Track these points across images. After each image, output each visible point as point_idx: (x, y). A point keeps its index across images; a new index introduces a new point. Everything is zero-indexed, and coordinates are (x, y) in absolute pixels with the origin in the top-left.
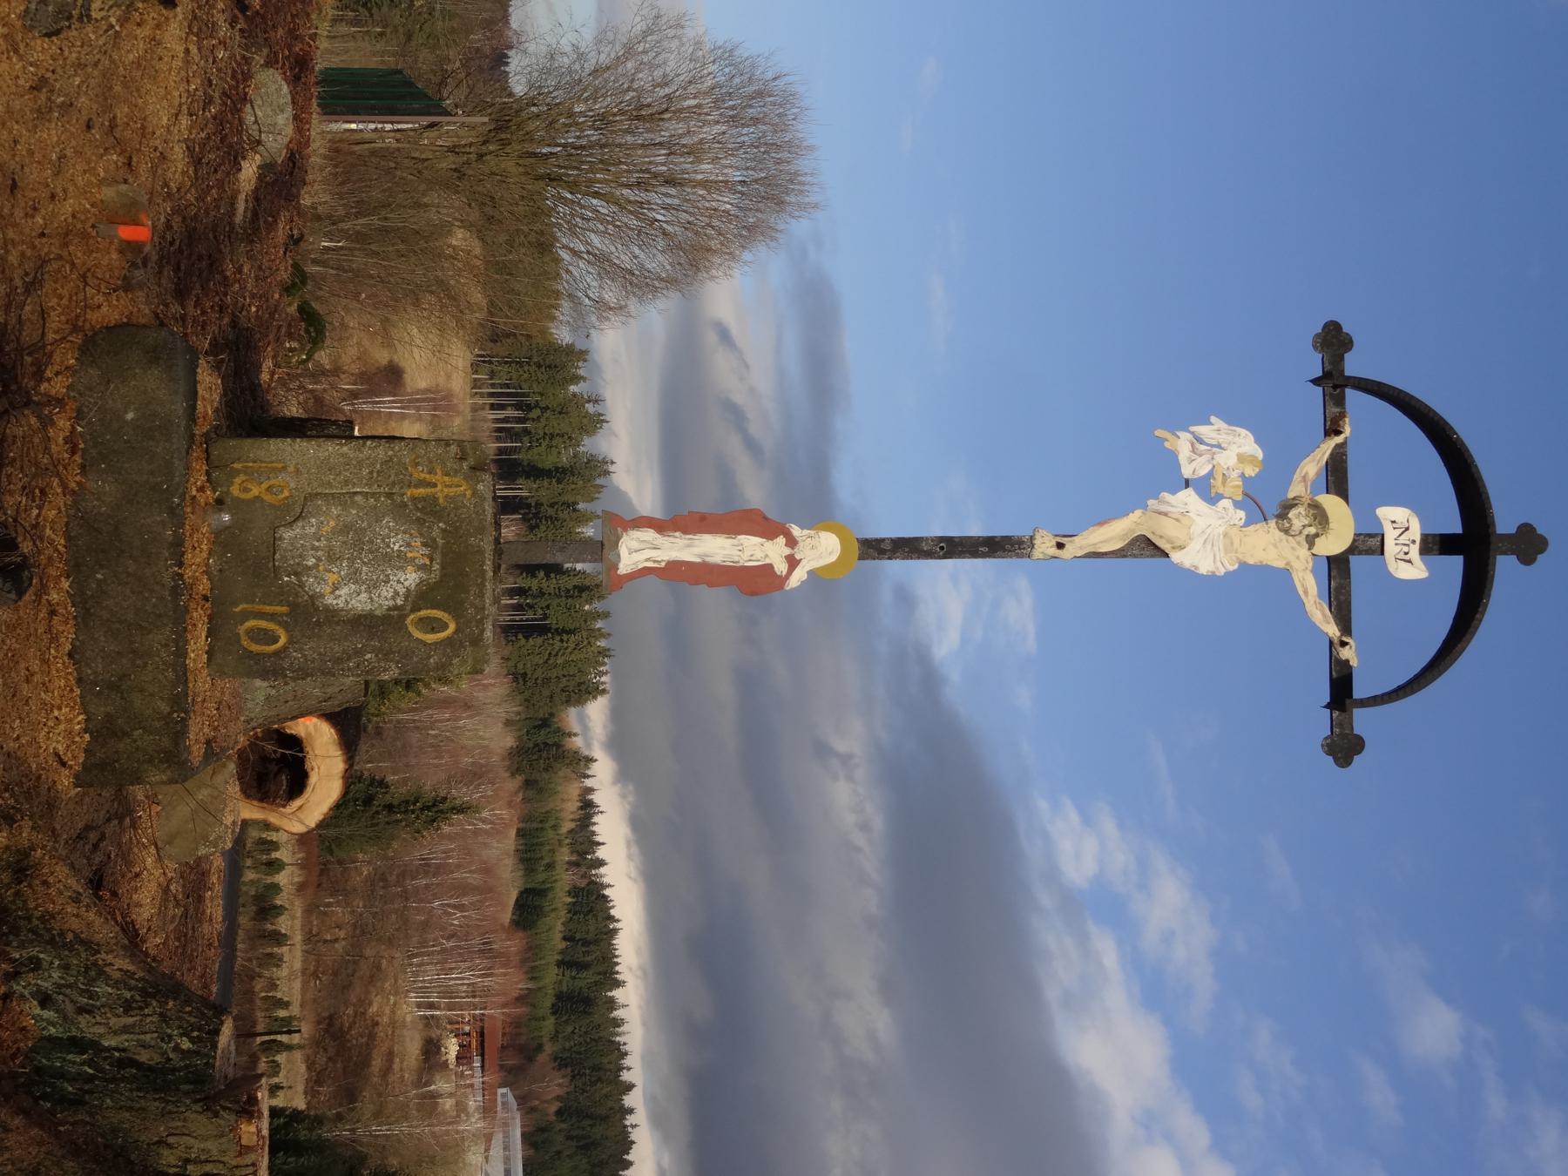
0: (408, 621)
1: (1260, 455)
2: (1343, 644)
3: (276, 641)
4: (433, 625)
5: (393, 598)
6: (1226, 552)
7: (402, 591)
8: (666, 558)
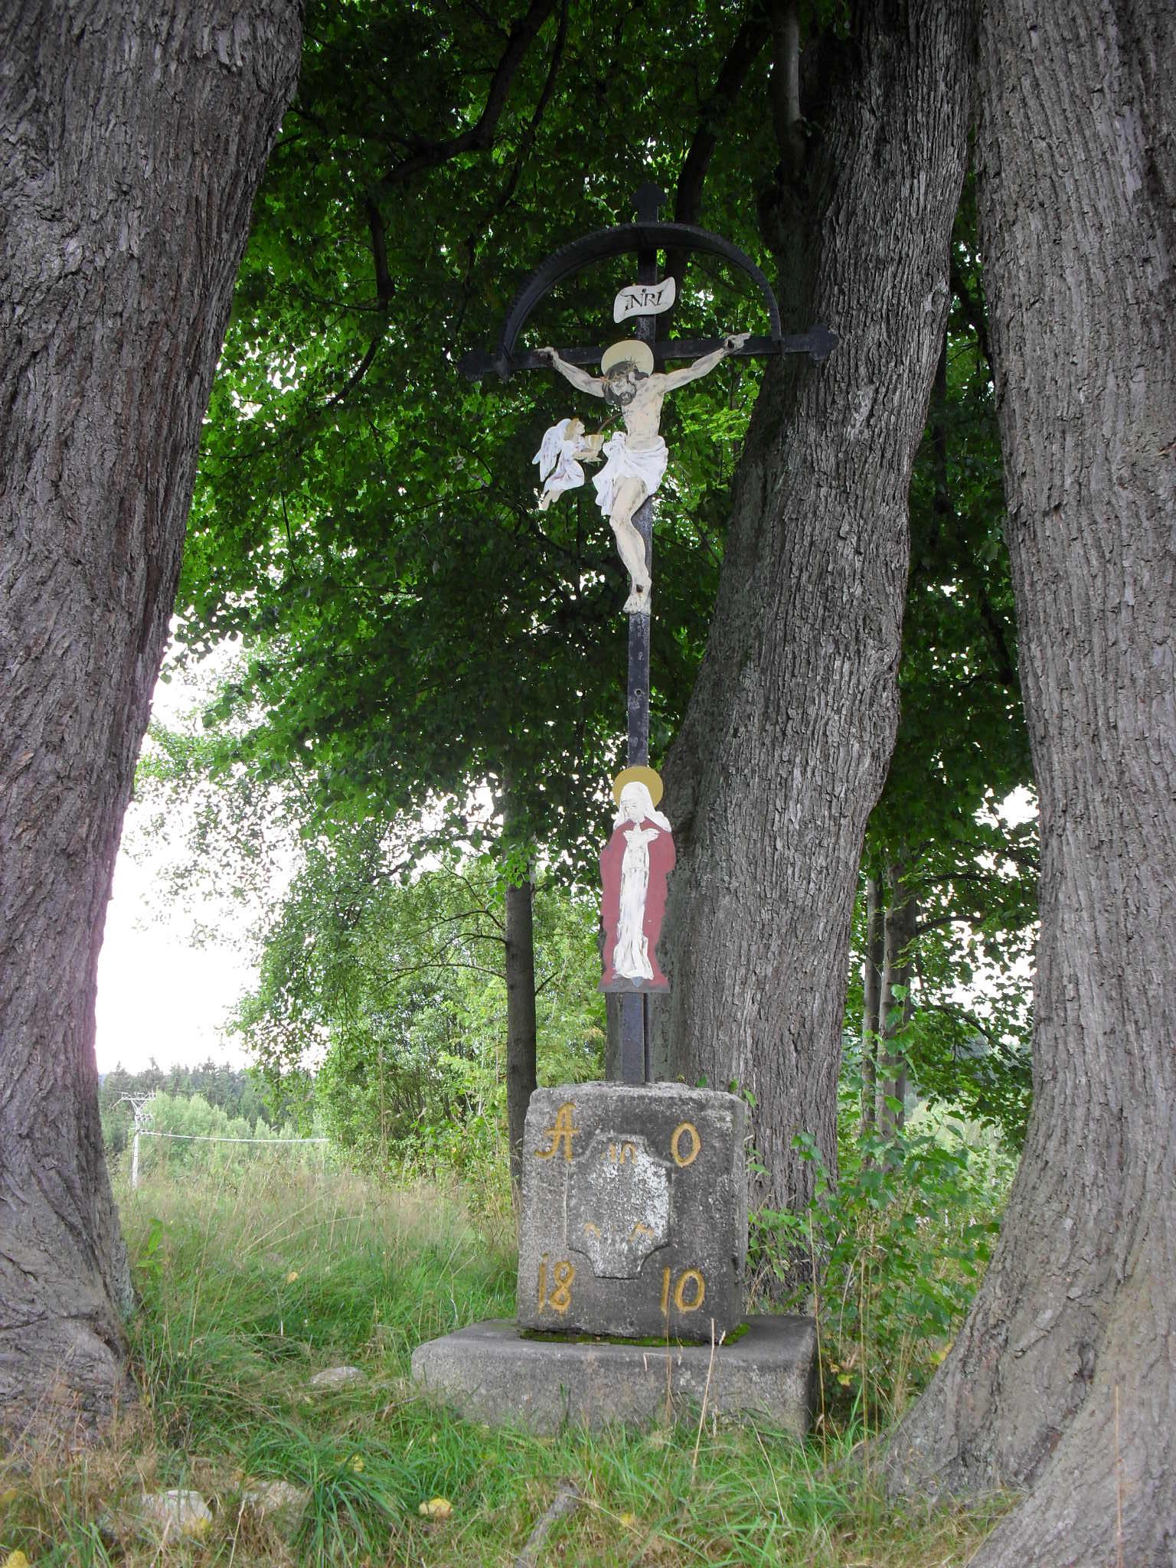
0: (681, 1165)
1: (566, 421)
2: (731, 345)
3: (693, 1281)
4: (685, 1148)
5: (659, 1177)
6: (648, 447)
7: (653, 1168)
8: (640, 936)
